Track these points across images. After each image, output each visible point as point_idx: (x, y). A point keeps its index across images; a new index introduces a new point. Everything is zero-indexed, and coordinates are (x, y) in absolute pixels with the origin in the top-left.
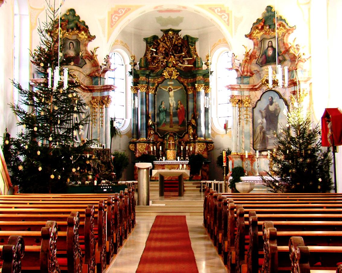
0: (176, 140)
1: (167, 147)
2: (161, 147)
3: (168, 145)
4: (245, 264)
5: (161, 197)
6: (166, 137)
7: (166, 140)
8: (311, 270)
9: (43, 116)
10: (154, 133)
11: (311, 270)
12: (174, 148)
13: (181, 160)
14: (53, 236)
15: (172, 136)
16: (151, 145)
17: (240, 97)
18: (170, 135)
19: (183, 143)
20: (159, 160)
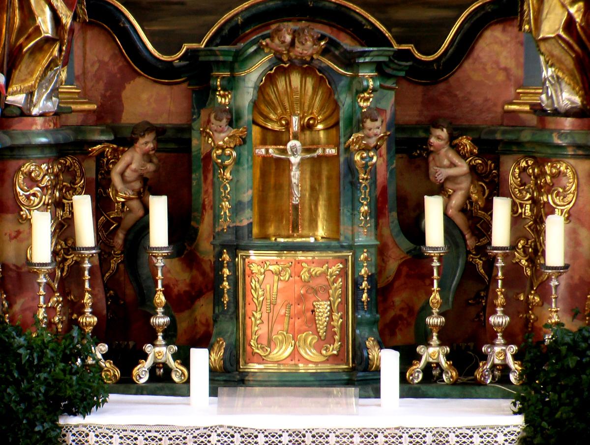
0: (356, 123)
1: (238, 208)
2: (159, 207)
3: (249, 177)
4: (435, 326)
5: (219, 395)
6: (231, 84)
7: (234, 120)
8: (426, 197)
9: (359, 64)
10: (67, 19)
11: (426, 197)
12: (335, 220)
13: (416, 374)
14: (105, 192)
15: (307, 68)
16: (32, 181)
17: (39, 179)
18: (278, 59)
19: (447, 155)
20: (141, 373)
